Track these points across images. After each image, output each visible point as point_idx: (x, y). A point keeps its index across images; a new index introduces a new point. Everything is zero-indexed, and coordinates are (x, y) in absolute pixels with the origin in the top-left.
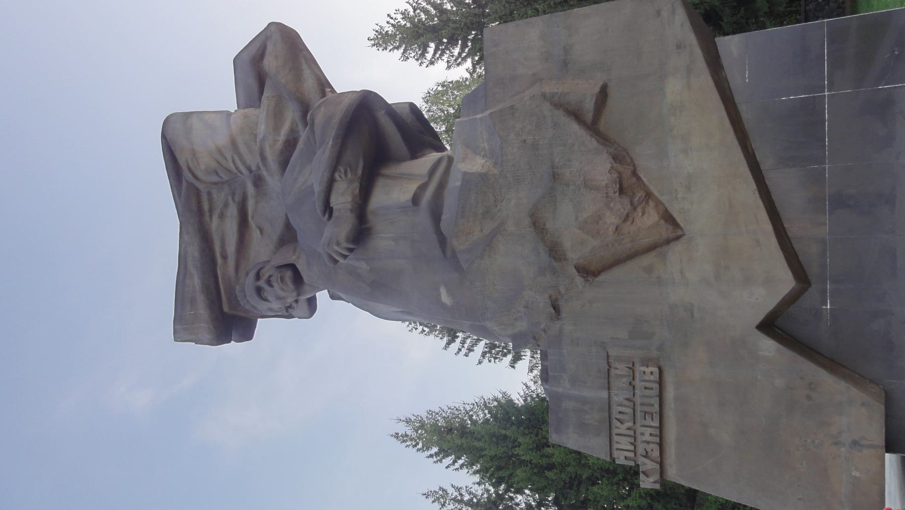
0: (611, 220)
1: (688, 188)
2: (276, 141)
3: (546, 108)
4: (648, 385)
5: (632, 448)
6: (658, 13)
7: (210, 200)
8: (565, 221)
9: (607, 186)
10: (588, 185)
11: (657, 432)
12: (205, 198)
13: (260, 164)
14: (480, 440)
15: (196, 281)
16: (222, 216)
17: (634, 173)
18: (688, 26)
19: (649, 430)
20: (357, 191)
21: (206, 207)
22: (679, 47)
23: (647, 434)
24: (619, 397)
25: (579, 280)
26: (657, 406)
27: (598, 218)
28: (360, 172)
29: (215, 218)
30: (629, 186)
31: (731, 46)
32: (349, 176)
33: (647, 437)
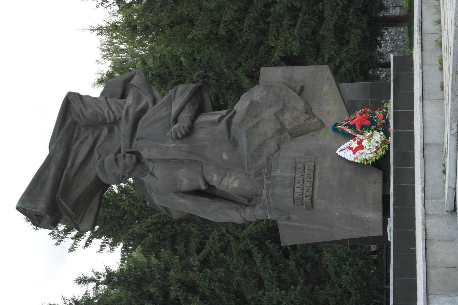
0: (302, 119)
1: (328, 114)
2: (136, 108)
3: (284, 86)
4: (310, 168)
5: (302, 191)
6: (322, 70)
7: (79, 133)
8: (287, 118)
9: (302, 110)
10: (296, 109)
11: (312, 183)
12: (77, 131)
13: (123, 118)
14: (322, 19)
15: (52, 172)
16: (82, 143)
17: (311, 109)
18: (331, 74)
19: (309, 183)
20: (194, 113)
21: (75, 135)
22: (328, 79)
23: (308, 184)
24: (298, 175)
25: (289, 137)
26: (312, 175)
27: (298, 118)
28: (196, 108)
29: (77, 143)
30: (308, 111)
31: (344, 85)
32: (192, 107)
33: (308, 185)
